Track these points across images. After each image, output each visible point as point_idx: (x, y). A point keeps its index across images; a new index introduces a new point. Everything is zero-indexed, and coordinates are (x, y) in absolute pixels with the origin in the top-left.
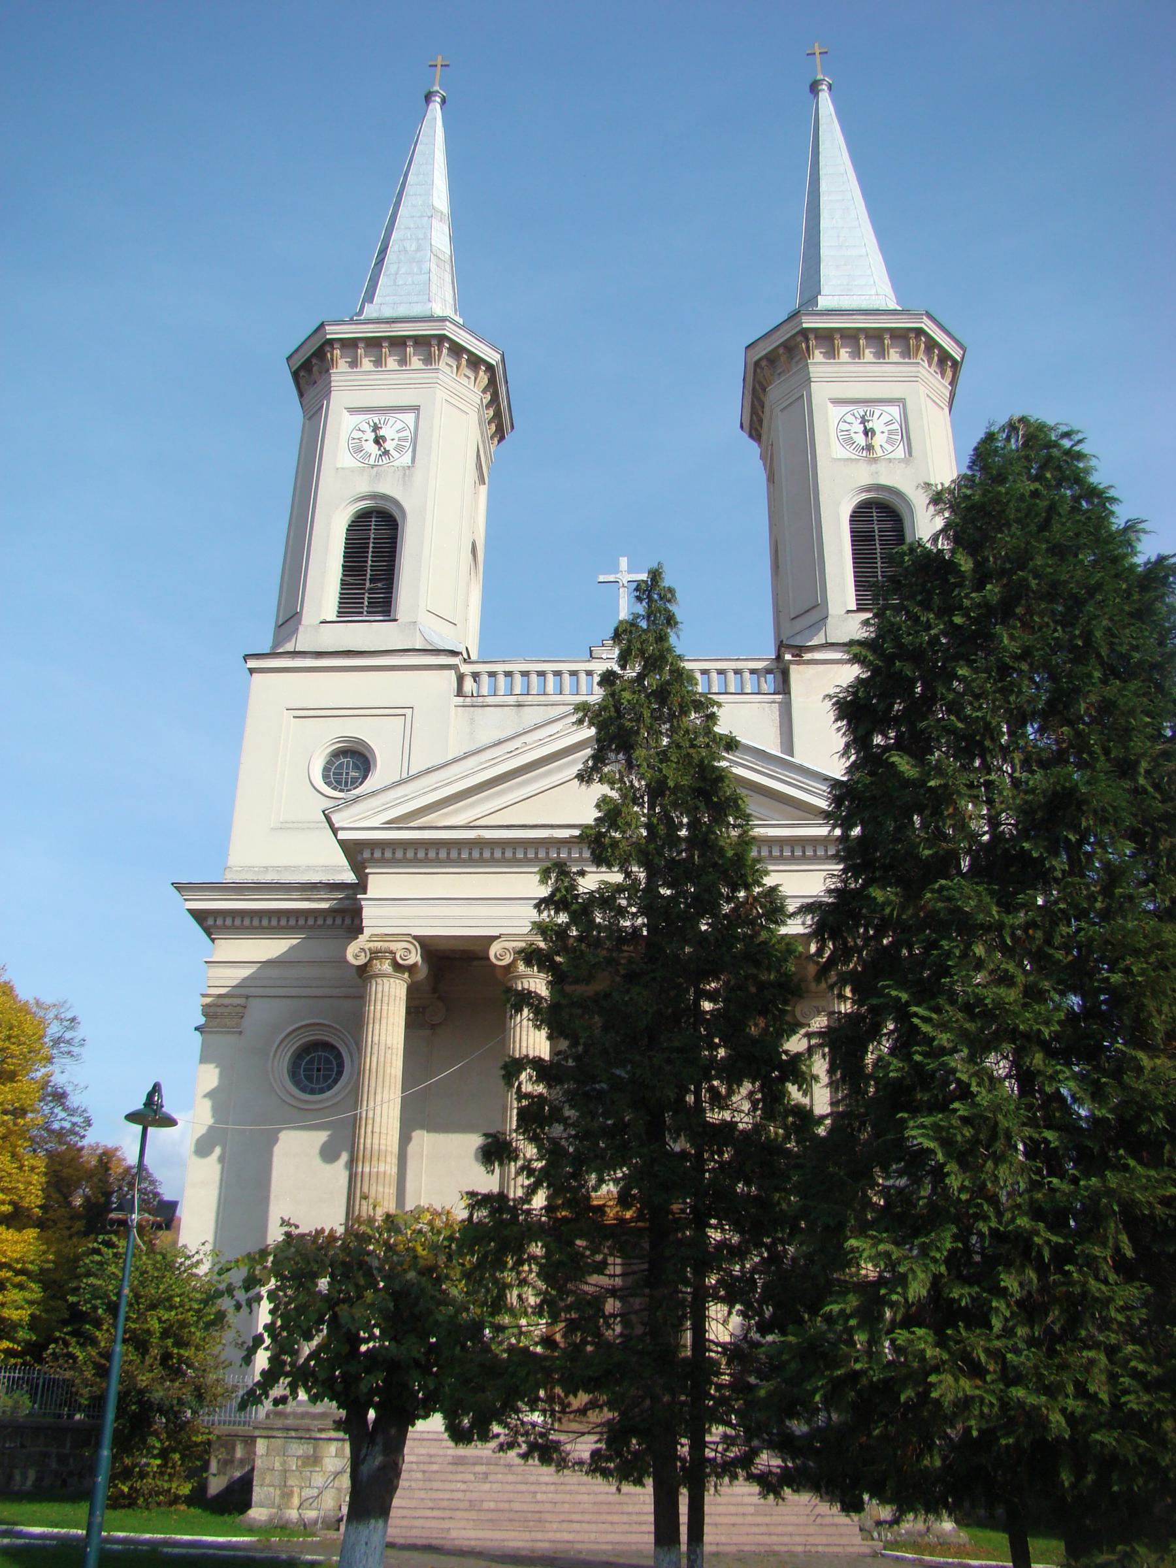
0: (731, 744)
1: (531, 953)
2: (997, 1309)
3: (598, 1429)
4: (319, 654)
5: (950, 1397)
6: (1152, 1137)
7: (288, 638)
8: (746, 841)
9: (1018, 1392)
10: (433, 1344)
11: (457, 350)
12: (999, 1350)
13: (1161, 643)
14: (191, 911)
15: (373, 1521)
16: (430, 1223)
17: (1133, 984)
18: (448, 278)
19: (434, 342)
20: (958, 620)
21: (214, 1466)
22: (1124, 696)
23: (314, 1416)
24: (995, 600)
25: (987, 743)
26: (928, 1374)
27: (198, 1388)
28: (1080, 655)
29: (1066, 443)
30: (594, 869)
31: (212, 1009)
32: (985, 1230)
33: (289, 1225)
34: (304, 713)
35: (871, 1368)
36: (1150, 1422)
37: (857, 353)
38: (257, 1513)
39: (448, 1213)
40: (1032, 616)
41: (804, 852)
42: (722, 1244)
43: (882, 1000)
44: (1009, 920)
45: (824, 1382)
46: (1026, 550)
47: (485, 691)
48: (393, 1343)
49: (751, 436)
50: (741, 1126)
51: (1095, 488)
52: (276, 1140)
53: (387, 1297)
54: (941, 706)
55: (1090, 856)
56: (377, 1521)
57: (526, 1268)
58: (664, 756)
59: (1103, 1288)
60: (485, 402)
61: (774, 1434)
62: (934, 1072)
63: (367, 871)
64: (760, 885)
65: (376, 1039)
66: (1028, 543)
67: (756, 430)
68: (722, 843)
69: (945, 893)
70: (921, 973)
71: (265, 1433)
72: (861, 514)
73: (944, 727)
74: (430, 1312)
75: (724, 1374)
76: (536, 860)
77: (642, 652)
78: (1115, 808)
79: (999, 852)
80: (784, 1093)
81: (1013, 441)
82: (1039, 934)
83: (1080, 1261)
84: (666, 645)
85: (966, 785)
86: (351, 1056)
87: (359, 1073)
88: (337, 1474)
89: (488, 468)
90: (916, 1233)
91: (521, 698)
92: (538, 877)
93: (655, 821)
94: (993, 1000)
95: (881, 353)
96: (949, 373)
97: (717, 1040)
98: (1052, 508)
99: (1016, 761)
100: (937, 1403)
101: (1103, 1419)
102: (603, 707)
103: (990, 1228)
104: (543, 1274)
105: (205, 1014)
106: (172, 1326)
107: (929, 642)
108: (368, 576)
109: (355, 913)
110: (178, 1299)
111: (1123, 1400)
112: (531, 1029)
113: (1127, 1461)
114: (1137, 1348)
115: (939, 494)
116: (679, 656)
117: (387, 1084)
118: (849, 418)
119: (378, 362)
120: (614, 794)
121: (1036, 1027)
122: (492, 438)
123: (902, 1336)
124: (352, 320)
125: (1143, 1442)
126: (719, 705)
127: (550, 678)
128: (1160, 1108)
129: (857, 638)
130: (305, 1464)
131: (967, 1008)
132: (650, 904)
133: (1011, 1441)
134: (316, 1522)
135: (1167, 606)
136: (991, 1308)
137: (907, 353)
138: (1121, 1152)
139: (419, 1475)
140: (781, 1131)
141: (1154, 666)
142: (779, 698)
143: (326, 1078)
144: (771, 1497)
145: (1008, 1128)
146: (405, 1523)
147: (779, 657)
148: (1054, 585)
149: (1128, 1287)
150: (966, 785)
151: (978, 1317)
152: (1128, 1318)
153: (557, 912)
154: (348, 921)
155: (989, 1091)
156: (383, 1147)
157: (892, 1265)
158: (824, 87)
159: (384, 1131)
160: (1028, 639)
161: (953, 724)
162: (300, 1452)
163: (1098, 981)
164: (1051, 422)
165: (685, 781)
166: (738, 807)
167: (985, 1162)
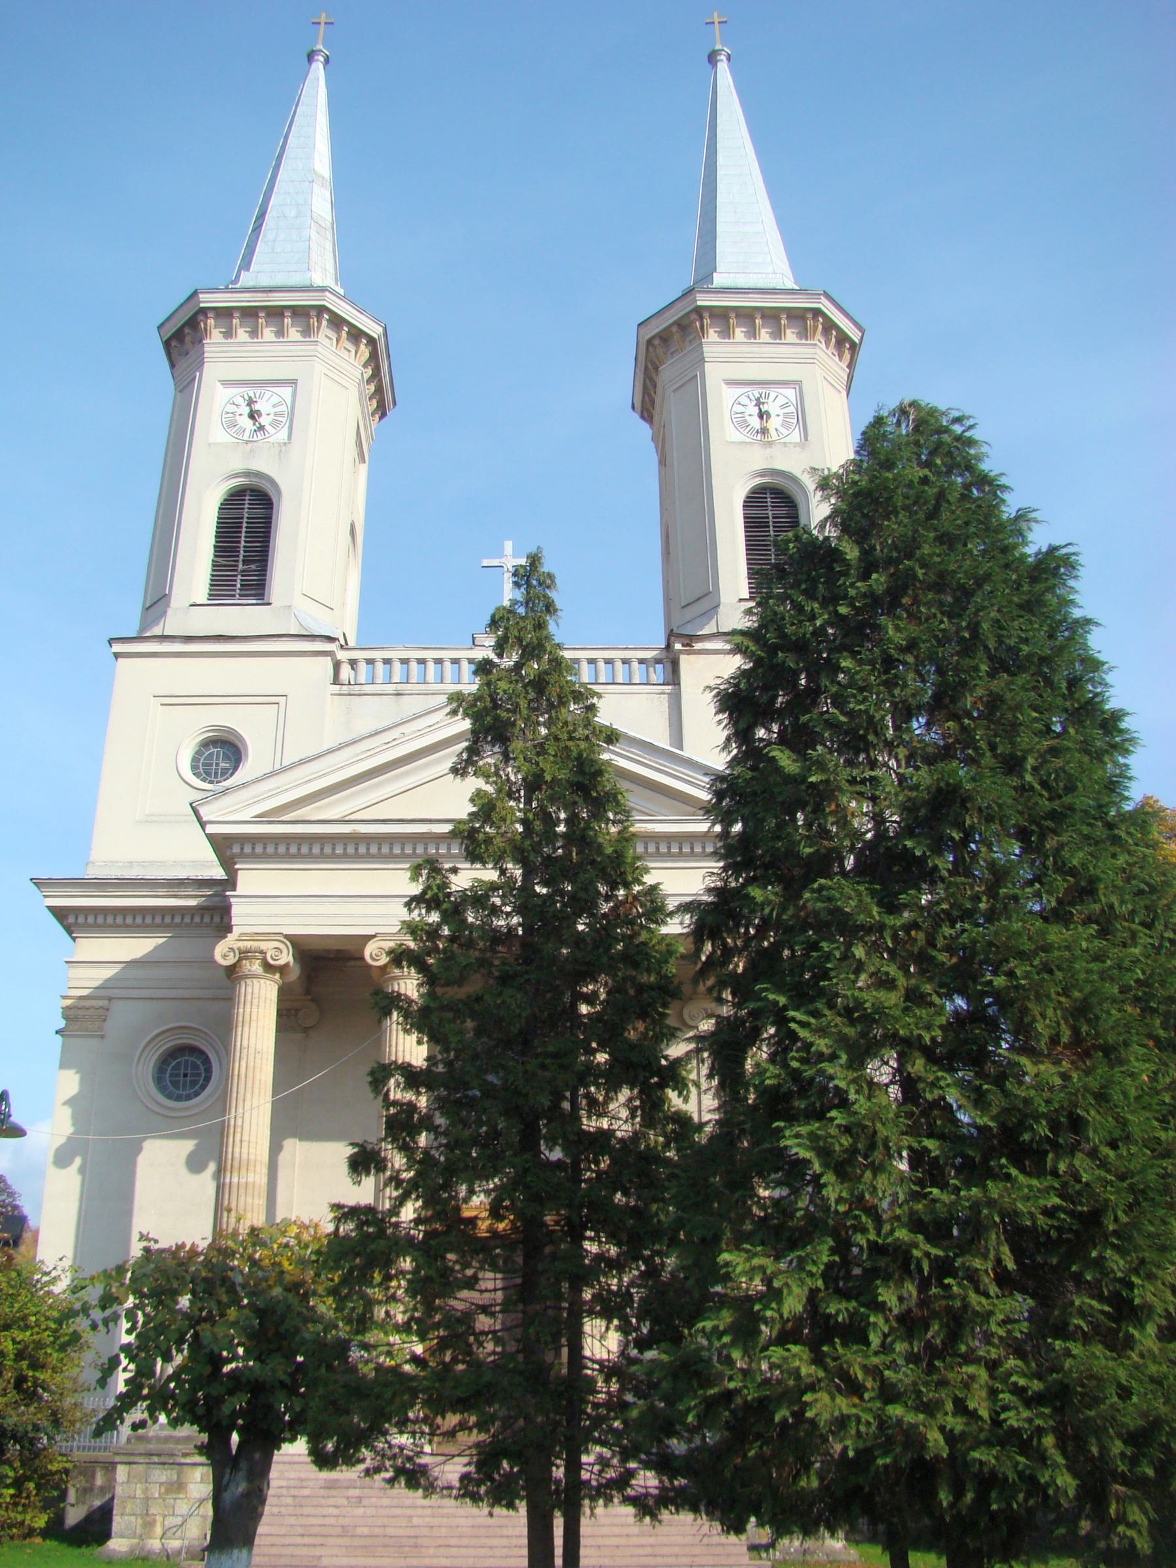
0: (612, 737)
1: (401, 953)
2: (875, 1324)
3: (467, 1452)
4: (189, 639)
5: (826, 1416)
6: (1035, 1146)
7: (155, 622)
8: (626, 838)
9: (895, 1410)
10: (300, 1363)
11: (337, 322)
12: (876, 1367)
13: (1051, 636)
14: (50, 908)
15: (236, 1552)
16: (298, 1237)
17: (1017, 988)
18: (329, 246)
19: (313, 313)
20: (843, 610)
21: (72, 1495)
22: (1011, 690)
23: (178, 1440)
24: (880, 589)
25: (871, 737)
26: (803, 1393)
27: (54, 1414)
28: (968, 648)
29: (957, 429)
30: (468, 865)
31: (72, 1012)
32: (863, 1242)
33: (149, 1240)
34: (172, 701)
35: (745, 1387)
36: (1030, 1438)
37: (753, 333)
38: (117, 1544)
39: (316, 1226)
40: (918, 607)
41: (692, 848)
42: (599, 1257)
43: (760, 1004)
44: (890, 920)
45: (697, 1401)
46: (914, 539)
47: (362, 678)
48: (258, 1364)
49: (642, 417)
50: (619, 1134)
51: (986, 476)
52: (140, 1150)
53: (252, 1315)
54: (826, 698)
55: (975, 855)
56: (240, 1551)
57: (394, 1283)
58: (541, 750)
59: (983, 1300)
60: (366, 376)
61: (652, 1454)
62: (812, 1079)
63: (237, 866)
64: (641, 883)
65: (245, 1043)
66: (917, 531)
67: (648, 411)
68: (601, 840)
69: (825, 893)
70: (802, 975)
71: (126, 1459)
72: (754, 499)
73: (826, 721)
74: (297, 1330)
75: (601, 1392)
76: (402, 857)
77: (519, 640)
78: (1000, 806)
79: (882, 850)
80: (663, 1100)
81: (903, 426)
82: (921, 936)
83: (960, 1274)
84: (545, 633)
85: (848, 781)
86: (220, 1061)
87: (227, 1080)
88: (202, 1501)
89: (369, 445)
90: (793, 1245)
91: (400, 687)
92: (408, 874)
93: (531, 816)
94: (873, 1004)
95: (778, 334)
96: (847, 356)
97: (594, 1045)
98: (941, 496)
99: (901, 756)
100: (813, 1422)
101: (982, 1436)
102: (478, 698)
103: (868, 1241)
104: (412, 1291)
105: (65, 1017)
106: (26, 1347)
107: (814, 633)
108: (241, 558)
109: (224, 910)
110: (33, 1319)
111: (1003, 1416)
112: (401, 1033)
113: (1006, 1479)
114: (1019, 1362)
115: (826, 479)
116: (558, 645)
117: (256, 1090)
118: (744, 400)
119: (254, 333)
120: (490, 789)
121: (916, 1032)
122: (373, 414)
123: (776, 1353)
124: (227, 288)
125: (1021, 1459)
126: (599, 696)
127: (431, 665)
128: (1044, 1115)
129: (739, 628)
130: (168, 1491)
131: (847, 1012)
132: (526, 905)
133: (888, 1460)
134: (179, 1552)
135: (1058, 597)
136: (869, 1323)
137: (804, 334)
138: (1003, 1161)
139: (289, 1501)
140: (661, 1139)
141: (1043, 660)
142: (668, 689)
143: (194, 1083)
144: (647, 1519)
145: (887, 1137)
146: (274, 1551)
147: (669, 647)
148: (941, 575)
149: (1008, 1300)
150: (848, 781)
151: (856, 1333)
152: (1009, 1332)
153: (428, 911)
154: (217, 919)
155: (869, 1098)
156: (252, 1157)
157: (768, 1281)
158: (723, 58)
159: (253, 1140)
160: (914, 630)
161: (836, 718)
162: (163, 1479)
163: (982, 984)
164: (943, 408)
165: (563, 775)
166: (618, 803)
167: (863, 1172)
